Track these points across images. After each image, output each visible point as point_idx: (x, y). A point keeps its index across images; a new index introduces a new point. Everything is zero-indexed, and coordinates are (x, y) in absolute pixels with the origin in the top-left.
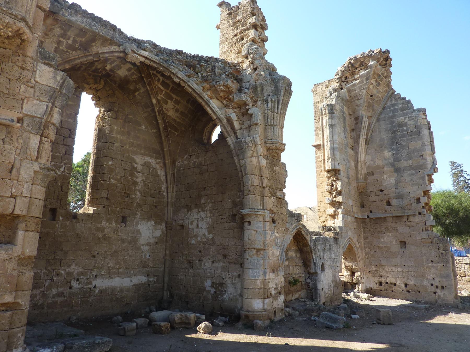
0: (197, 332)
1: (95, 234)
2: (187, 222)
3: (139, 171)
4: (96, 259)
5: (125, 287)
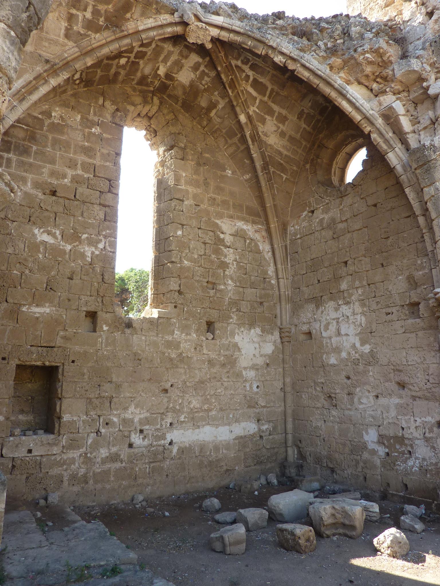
0: (375, 551)
1: (164, 353)
2: (317, 326)
3: (228, 244)
4: (168, 395)
5: (221, 441)
